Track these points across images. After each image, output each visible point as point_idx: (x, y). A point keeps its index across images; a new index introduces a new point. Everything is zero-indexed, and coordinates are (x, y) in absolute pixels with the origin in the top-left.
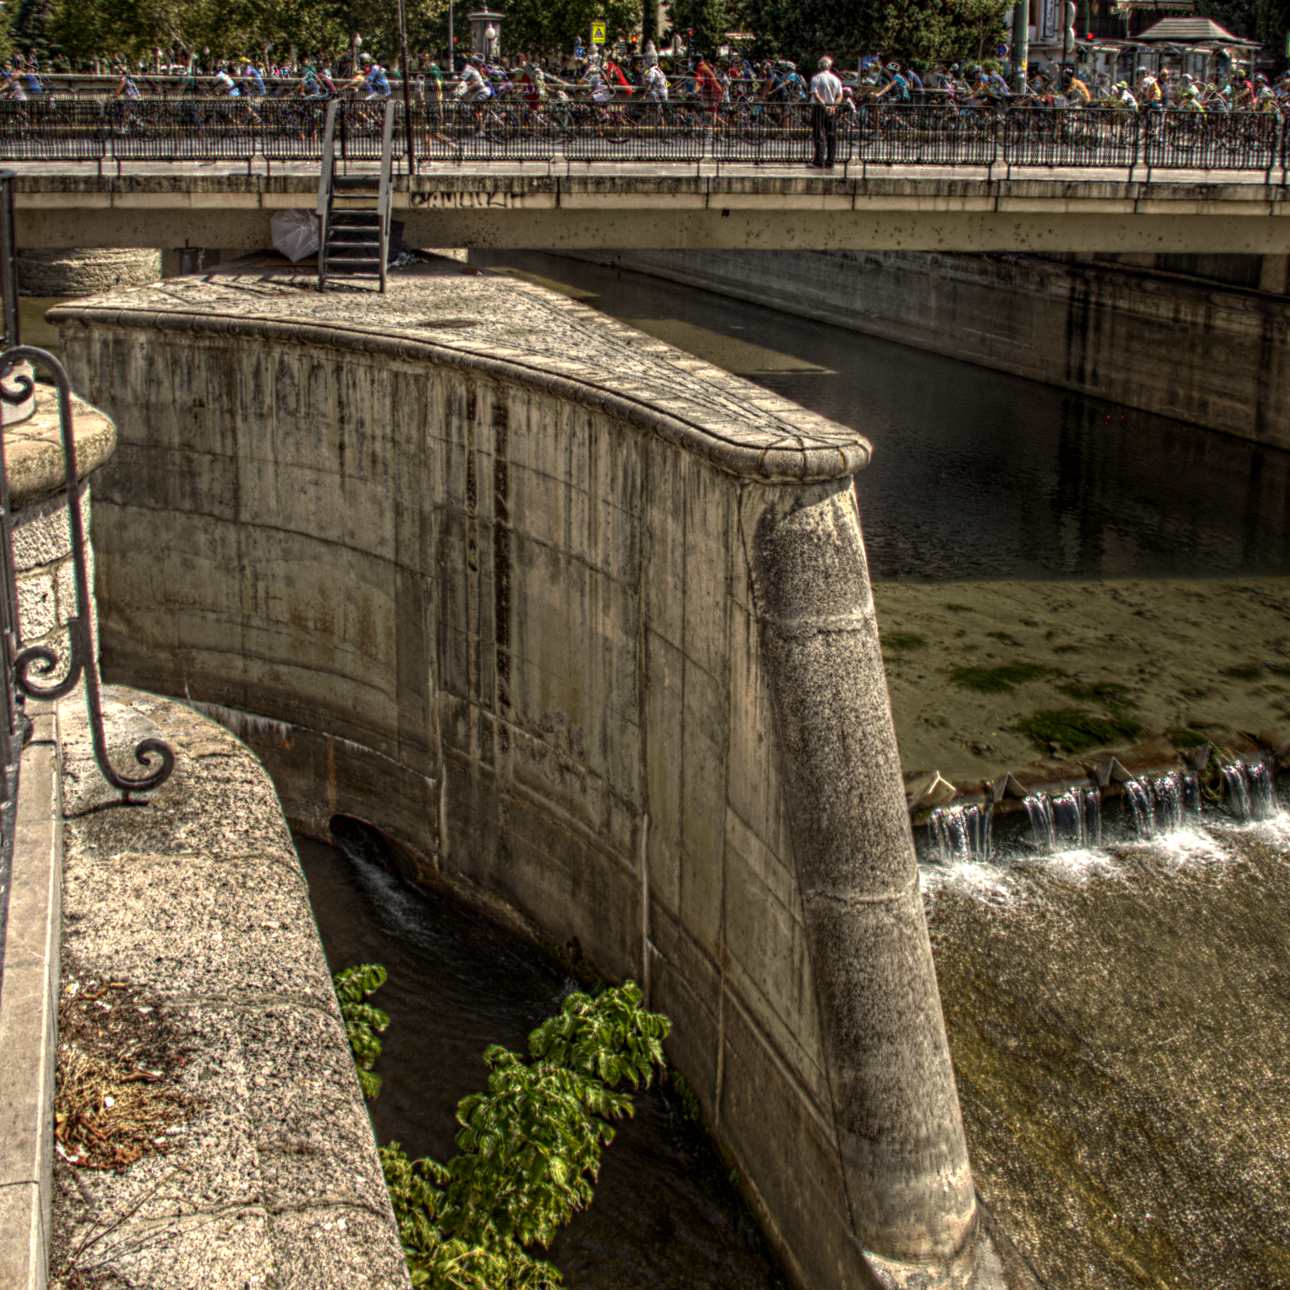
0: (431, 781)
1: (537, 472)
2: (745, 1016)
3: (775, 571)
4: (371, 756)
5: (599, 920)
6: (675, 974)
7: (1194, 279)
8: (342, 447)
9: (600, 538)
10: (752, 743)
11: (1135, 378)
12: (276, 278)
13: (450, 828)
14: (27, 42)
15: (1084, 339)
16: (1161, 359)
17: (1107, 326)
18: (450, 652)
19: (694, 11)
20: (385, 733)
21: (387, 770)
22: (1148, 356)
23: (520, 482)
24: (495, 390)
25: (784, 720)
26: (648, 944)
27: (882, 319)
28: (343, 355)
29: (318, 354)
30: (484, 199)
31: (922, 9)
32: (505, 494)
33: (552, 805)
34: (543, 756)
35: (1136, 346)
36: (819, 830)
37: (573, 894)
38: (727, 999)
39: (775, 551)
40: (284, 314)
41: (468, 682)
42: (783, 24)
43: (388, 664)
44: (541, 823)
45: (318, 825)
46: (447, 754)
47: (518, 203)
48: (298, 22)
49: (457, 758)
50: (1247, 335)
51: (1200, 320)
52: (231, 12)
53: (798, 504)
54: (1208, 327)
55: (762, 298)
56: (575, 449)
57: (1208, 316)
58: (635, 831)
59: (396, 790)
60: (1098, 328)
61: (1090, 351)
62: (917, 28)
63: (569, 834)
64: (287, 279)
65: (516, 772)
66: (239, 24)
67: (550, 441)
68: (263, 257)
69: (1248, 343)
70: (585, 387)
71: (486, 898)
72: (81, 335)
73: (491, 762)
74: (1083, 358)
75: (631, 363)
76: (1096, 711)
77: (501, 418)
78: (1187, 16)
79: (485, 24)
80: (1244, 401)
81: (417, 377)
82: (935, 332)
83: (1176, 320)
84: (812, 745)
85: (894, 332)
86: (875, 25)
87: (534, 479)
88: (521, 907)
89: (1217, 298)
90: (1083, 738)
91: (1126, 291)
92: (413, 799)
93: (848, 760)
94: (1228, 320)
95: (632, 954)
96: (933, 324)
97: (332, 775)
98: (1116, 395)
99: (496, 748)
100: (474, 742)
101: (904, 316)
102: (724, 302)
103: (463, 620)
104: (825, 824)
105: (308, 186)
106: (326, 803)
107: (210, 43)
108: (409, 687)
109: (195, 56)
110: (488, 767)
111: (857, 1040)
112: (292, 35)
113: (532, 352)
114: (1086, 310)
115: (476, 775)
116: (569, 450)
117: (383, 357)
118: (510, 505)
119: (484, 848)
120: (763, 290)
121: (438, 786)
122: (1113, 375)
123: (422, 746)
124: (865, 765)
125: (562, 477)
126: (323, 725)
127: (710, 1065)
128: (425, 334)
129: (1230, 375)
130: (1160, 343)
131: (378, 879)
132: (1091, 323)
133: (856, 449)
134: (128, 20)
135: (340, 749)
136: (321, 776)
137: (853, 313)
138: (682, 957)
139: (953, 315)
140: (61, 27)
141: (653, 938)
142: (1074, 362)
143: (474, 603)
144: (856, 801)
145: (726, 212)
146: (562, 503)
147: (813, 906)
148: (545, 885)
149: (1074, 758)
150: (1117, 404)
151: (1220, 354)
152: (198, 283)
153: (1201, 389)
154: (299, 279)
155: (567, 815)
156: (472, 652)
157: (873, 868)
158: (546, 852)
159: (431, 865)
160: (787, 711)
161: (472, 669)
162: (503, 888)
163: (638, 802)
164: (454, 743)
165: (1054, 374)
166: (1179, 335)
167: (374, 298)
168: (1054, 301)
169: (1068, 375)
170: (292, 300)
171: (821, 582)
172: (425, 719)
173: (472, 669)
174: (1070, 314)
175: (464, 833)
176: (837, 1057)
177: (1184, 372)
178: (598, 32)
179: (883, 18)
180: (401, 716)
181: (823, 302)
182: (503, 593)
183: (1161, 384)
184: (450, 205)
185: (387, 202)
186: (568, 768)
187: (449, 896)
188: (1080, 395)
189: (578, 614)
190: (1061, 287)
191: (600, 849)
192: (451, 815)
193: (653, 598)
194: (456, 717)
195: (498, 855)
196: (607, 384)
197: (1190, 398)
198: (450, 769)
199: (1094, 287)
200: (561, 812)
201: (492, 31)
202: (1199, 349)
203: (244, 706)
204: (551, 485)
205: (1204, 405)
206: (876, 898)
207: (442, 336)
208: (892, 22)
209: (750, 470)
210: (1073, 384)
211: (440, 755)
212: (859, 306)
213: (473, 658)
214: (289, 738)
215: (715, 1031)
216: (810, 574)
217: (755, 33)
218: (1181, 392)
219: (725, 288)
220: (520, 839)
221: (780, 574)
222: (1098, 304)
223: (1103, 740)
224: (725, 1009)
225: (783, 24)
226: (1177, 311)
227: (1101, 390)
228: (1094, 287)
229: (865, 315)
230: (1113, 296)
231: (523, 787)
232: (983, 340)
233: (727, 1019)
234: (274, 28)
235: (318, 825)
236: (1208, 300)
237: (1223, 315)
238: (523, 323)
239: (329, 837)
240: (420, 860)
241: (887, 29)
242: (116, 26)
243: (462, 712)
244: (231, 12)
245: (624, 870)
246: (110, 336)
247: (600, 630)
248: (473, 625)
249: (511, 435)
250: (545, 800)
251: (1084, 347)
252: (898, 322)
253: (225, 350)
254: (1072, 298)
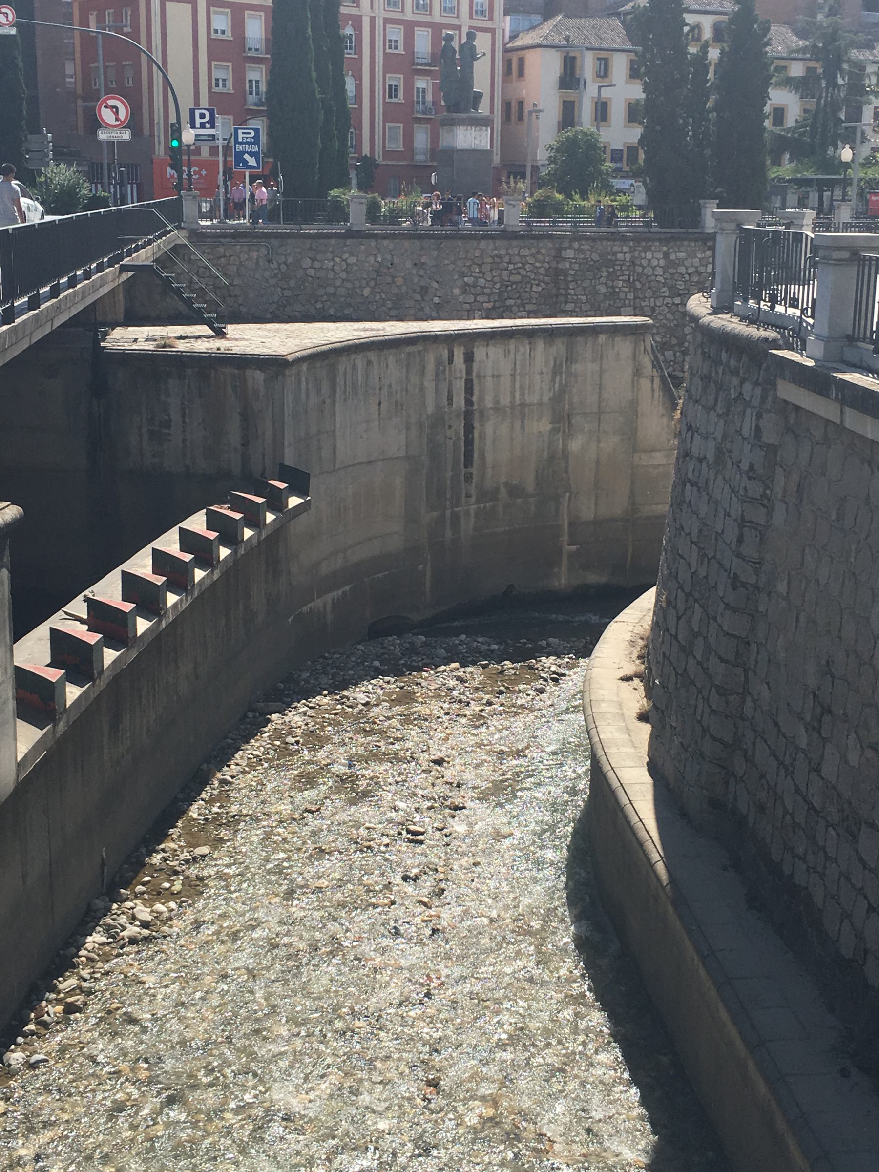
8: (380, 404)
29: (372, 355)
32: (472, 394)
77: (469, 358)
81: (419, 352)
118: (475, 399)
182: (469, 443)
193: (575, 399)
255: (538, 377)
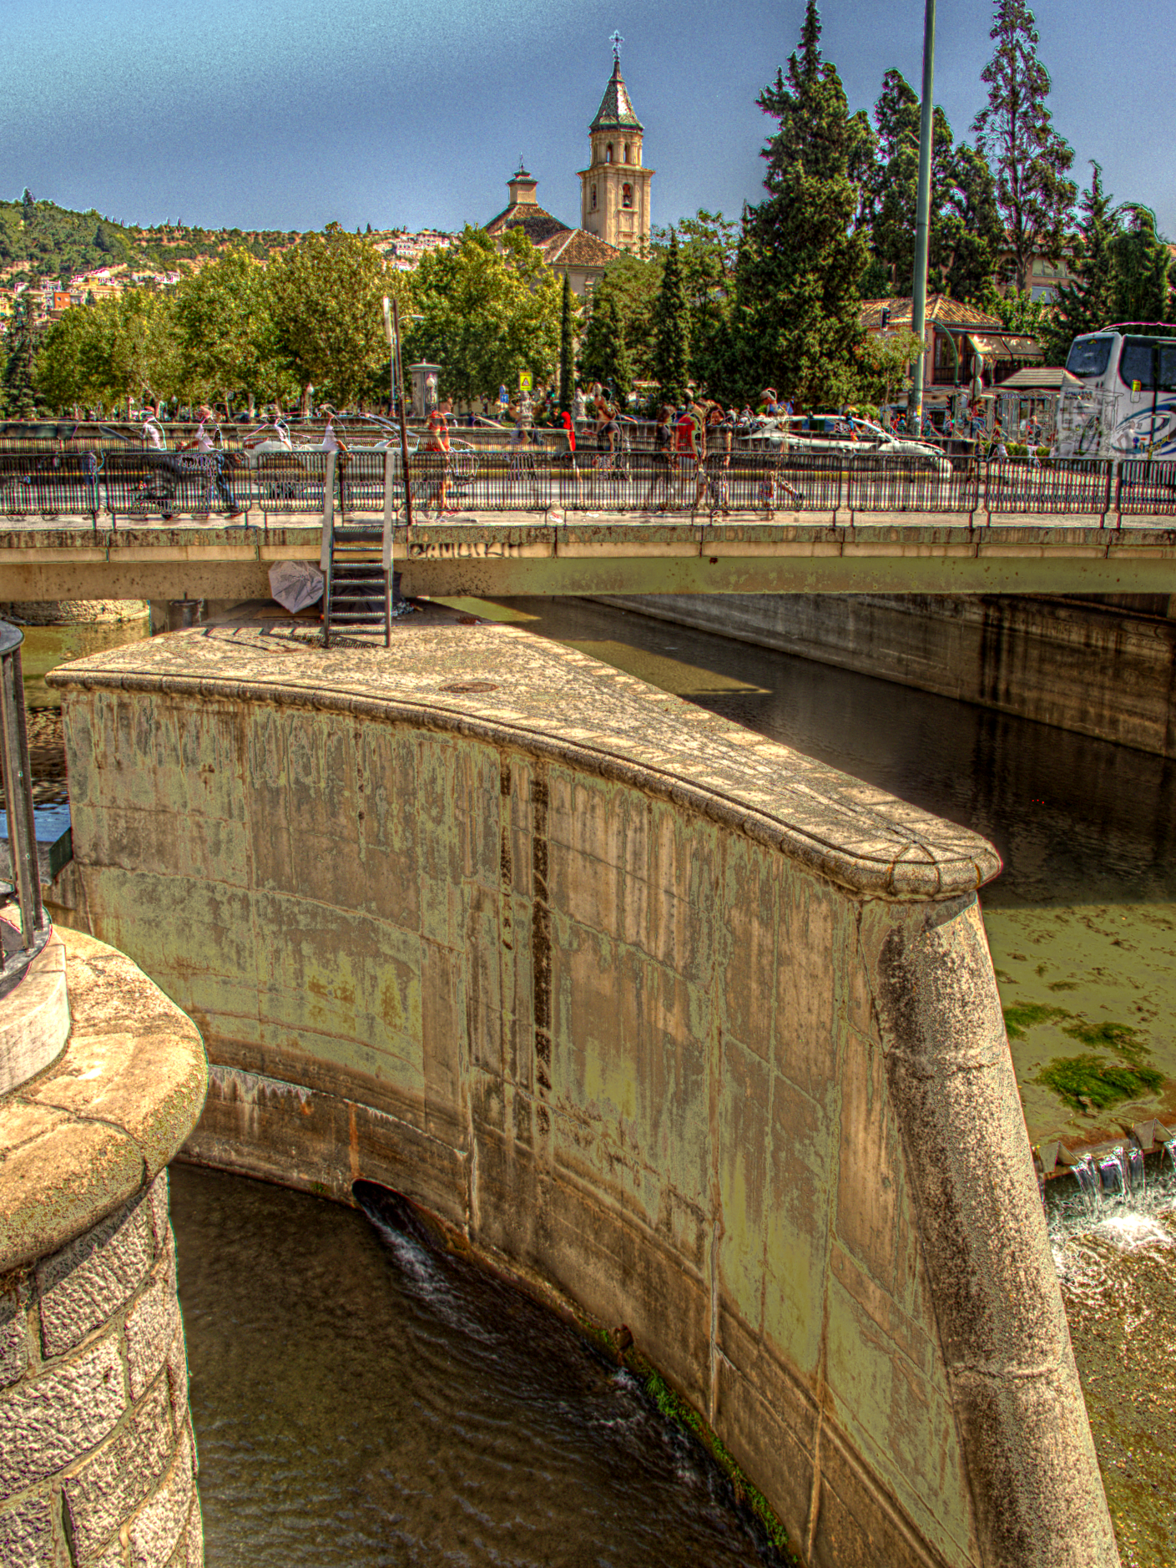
0: (461, 1155)
1: (583, 853)
2: (854, 1464)
3: (905, 1005)
4: (397, 1126)
5: (656, 1316)
6: (753, 1391)
7: (1103, 607)
9: (662, 931)
10: (872, 1182)
11: (1047, 697)
12: (276, 631)
13: (482, 1202)
14: (15, 392)
15: (998, 661)
16: (1073, 681)
17: (1020, 649)
18: (482, 1029)
19: (607, 363)
20: (412, 1105)
21: (414, 1140)
22: (1059, 677)
23: (562, 862)
24: (534, 765)
25: (921, 1170)
26: (716, 1355)
27: (802, 640)
28: (361, 722)
30: (482, 549)
31: (831, 360)
33: (600, 1194)
34: (588, 1143)
35: (1048, 668)
36: (968, 1297)
37: (623, 1284)
38: (824, 1434)
39: (905, 979)
40: (293, 676)
41: (503, 1060)
42: (706, 375)
43: (72, 537)
44: (586, 1209)
45: (340, 1189)
46: (477, 1128)
47: (515, 553)
48: (256, 373)
49: (491, 1134)
50: (1156, 659)
51: (1111, 645)
52: (196, 365)
53: (929, 924)
54: (1118, 652)
55: (690, 621)
56: (630, 834)
57: (1119, 642)
58: (701, 1236)
59: (423, 1160)
60: (1011, 651)
61: (1003, 672)
62: (827, 378)
63: (619, 1223)
64: (287, 631)
65: (558, 1158)
66: (204, 376)
67: (600, 824)
68: (259, 608)
69: (1158, 667)
70: (646, 771)
71: (522, 1273)
72: (83, 697)
73: (529, 1141)
74: (997, 678)
75: (682, 738)
76: (1110, 1058)
77: (541, 794)
78: (1038, 365)
79: (425, 374)
80: (1155, 720)
82: (854, 652)
83: (1088, 645)
84: (956, 1201)
85: (815, 653)
86: (790, 375)
87: (580, 861)
88: (563, 1288)
89: (1129, 626)
90: (1109, 1091)
91: (1038, 619)
92: (442, 1170)
93: (997, 1214)
94: (1139, 646)
95: (696, 1356)
96: (851, 645)
97: (355, 1141)
98: (1029, 712)
99: (535, 1130)
100: (509, 1122)
101: (823, 638)
102: (652, 624)
103: (496, 998)
104: (974, 1290)
105: (307, 537)
106: (349, 1168)
107: (177, 392)
108: (439, 1061)
109: (162, 403)
110: (524, 1146)
111: (1022, 1537)
112: (251, 385)
113: (569, 723)
114: (999, 634)
115: (512, 1154)
116: (622, 833)
117: (406, 725)
118: (551, 885)
119: (520, 1225)
120: (689, 613)
121: (469, 1159)
122: (1027, 694)
123: (451, 1120)
124: (1016, 1218)
125: (614, 862)
126: (344, 1091)
127: (800, 1494)
128: (450, 700)
129: (1140, 696)
130: (1071, 666)
131: (408, 1253)
132: (1005, 646)
133: (959, 852)
134: (104, 373)
135: (362, 1117)
136: (343, 1139)
137: (773, 634)
138: (761, 1374)
139: (870, 637)
140: (45, 379)
141: (724, 1348)
142: (988, 682)
143: (508, 981)
144: (1008, 1261)
145: (714, 560)
146: (613, 889)
147: (962, 1381)
148: (590, 1269)
149: (1105, 1115)
150: (1029, 720)
151: (1130, 677)
152: (199, 638)
153: (1111, 708)
154: (300, 631)
155: (618, 1206)
156: (507, 1030)
157: (1030, 1336)
158: (592, 1238)
159: (461, 1236)
160: (926, 1161)
161: (507, 1048)
162: (539, 1263)
163: (705, 1205)
164: (486, 1119)
165: (970, 692)
166: (1090, 659)
167: (381, 654)
168: (969, 626)
169: (982, 693)
170: (300, 658)
171: (957, 1012)
172: (454, 1093)
173: (507, 1048)
174: (984, 638)
175: (497, 1207)
176: (997, 1555)
177: (1095, 692)
178: (526, 379)
179: (798, 368)
180: (428, 1088)
181: (746, 624)
183: (1074, 703)
184: (447, 555)
185: (391, 554)
186: (619, 1160)
187: (473, 1264)
188: (996, 712)
189: (633, 1006)
190: (975, 615)
191: (658, 1246)
192: (485, 1188)
194: (489, 1093)
195: (536, 1233)
196: (669, 767)
197: (1100, 717)
198: (482, 1144)
199: (1007, 614)
200: (609, 1200)
201: (432, 381)
202: (1110, 672)
203: (262, 1070)
204: (600, 868)
205: (1114, 722)
206: (1035, 1371)
207: (466, 703)
208: (804, 372)
209: (874, 887)
210: (987, 701)
211: (471, 1129)
212: (780, 628)
213: (509, 1037)
214: (308, 1103)
215: (807, 1465)
216: (946, 1003)
217: (660, 381)
218: (1092, 710)
219: (653, 610)
220: (562, 1220)
221: (911, 1004)
222: (1011, 629)
223: (1130, 1094)
224: (823, 1447)
225: (706, 375)
226: (1088, 637)
227: (1015, 708)
228: (1007, 614)
229: (786, 637)
230: (1025, 622)
231: (563, 1170)
232: (900, 660)
233: (826, 1458)
234: (234, 379)
235: (340, 1189)
236: (1120, 627)
237: (1134, 641)
238: (534, 684)
239: (352, 1201)
240: (450, 1230)
241: (801, 379)
242: (93, 379)
243: (495, 1089)
244: (196, 365)
245: (687, 1272)
246: (114, 701)
247: (661, 1025)
248: (508, 1005)
249: (551, 816)
250: (592, 1188)
251: (997, 668)
252: (818, 643)
253: (236, 715)
254: (985, 624)
255: (663, 897)
